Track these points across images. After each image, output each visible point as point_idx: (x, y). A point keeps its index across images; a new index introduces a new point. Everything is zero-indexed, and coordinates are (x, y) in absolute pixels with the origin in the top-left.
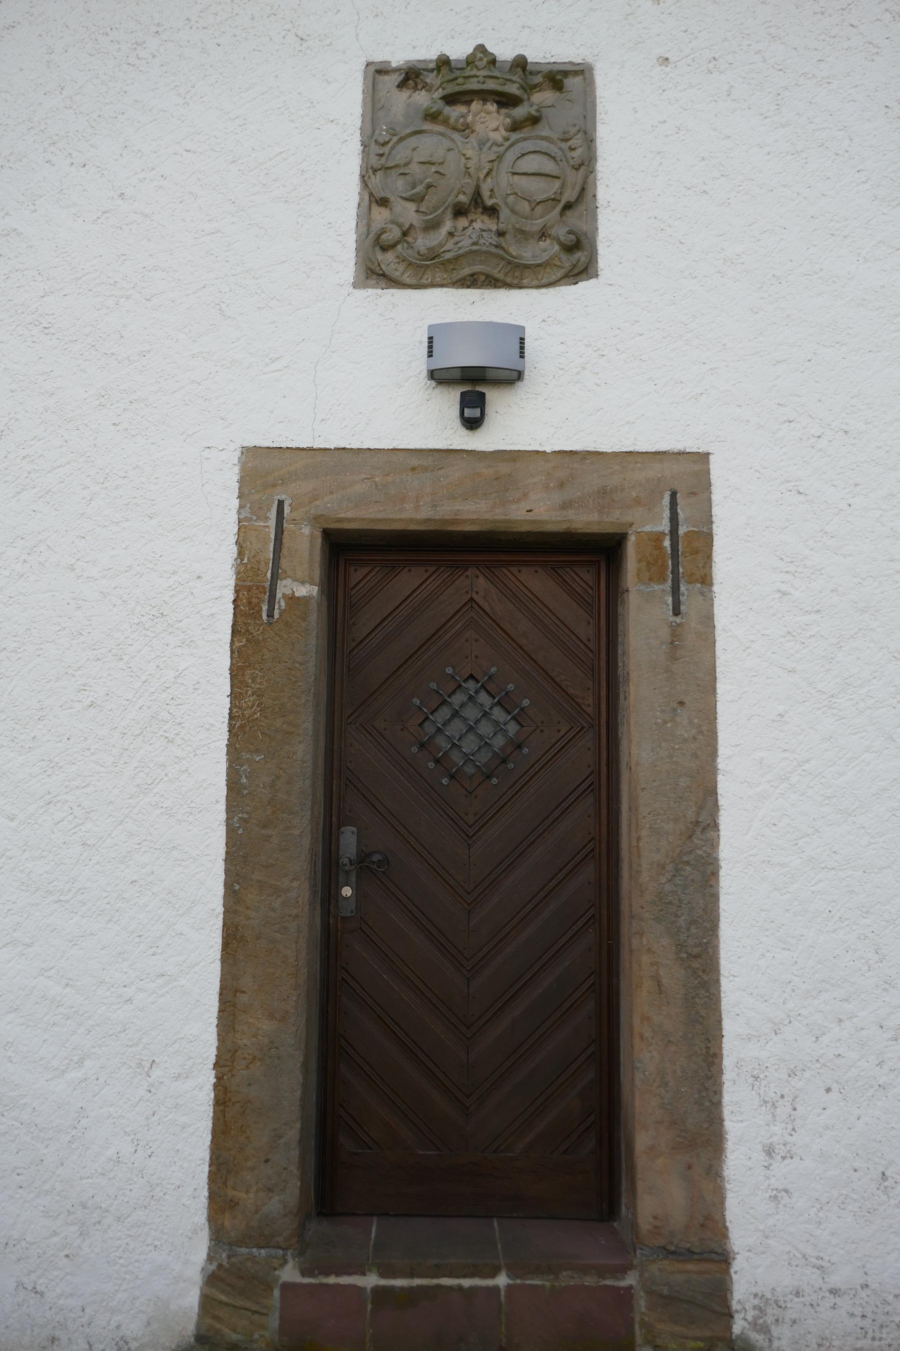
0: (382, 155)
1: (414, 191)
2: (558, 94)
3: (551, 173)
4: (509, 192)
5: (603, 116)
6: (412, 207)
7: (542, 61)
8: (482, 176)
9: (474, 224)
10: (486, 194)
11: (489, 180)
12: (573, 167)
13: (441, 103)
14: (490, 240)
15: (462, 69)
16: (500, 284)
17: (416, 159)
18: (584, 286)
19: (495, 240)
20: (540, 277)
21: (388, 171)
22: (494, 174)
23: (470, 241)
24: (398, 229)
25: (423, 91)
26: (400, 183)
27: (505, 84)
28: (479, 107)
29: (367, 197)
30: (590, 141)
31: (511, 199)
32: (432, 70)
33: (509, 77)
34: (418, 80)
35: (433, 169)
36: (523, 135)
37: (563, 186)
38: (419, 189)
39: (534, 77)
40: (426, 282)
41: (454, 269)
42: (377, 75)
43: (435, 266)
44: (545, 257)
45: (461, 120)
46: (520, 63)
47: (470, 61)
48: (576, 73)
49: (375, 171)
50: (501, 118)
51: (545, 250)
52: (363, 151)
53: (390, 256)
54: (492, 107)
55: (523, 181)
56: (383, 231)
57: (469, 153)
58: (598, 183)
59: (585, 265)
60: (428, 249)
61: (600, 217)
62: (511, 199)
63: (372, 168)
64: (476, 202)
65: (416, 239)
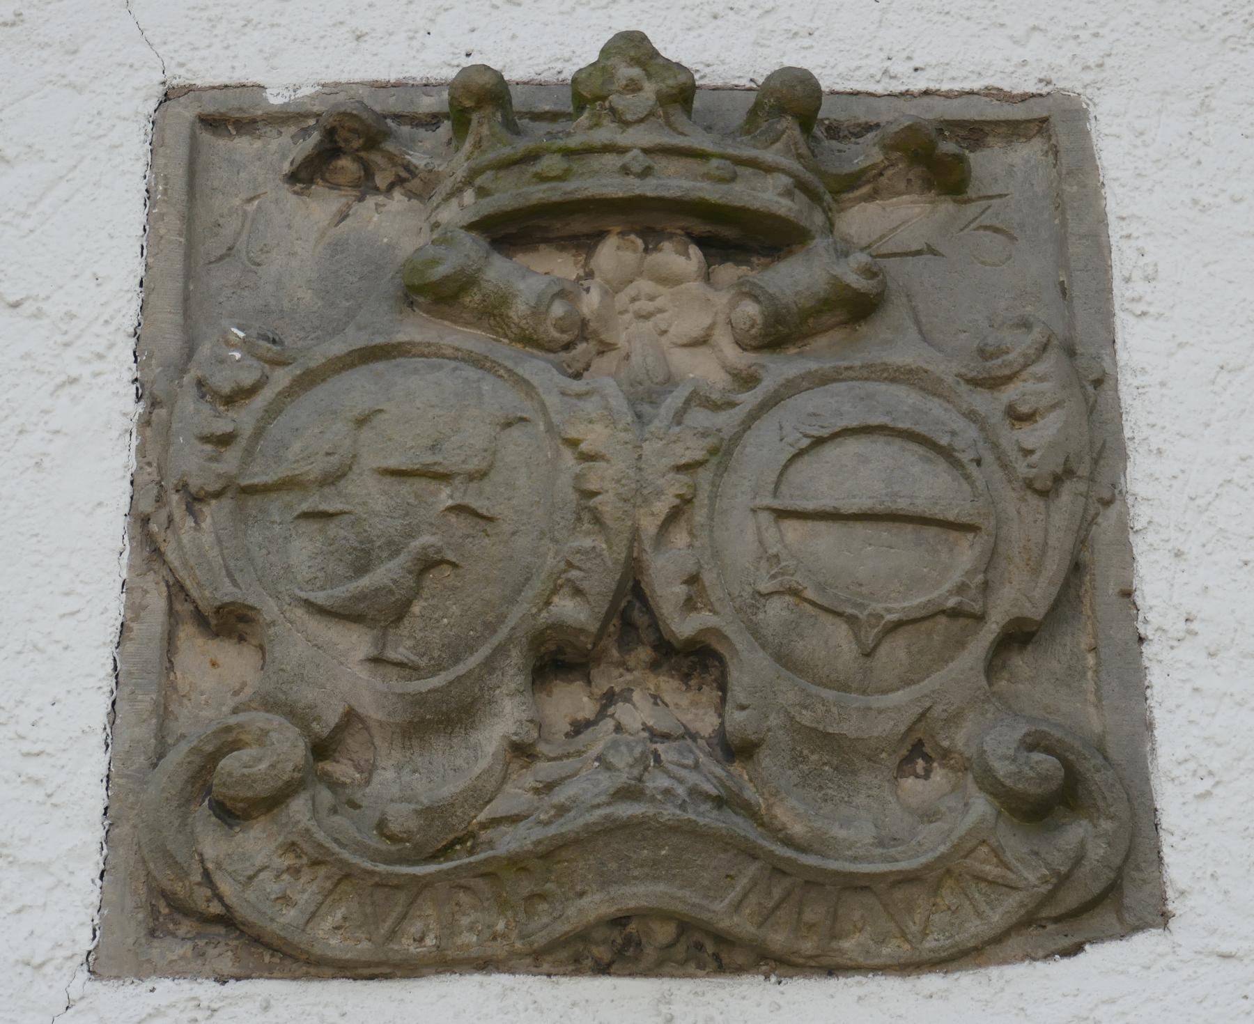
0: (225, 440)
1: (365, 582)
2: (946, 207)
3: (937, 512)
4: (765, 586)
5: (1139, 287)
6: (355, 643)
7: (879, 89)
8: (649, 526)
9: (621, 711)
10: (667, 592)
11: (680, 538)
12: (1029, 485)
13: (471, 248)
14: (693, 778)
15: (553, 116)
16: (740, 959)
17: (370, 460)
18: (1108, 967)
19: (711, 774)
20: (914, 929)
21: (253, 502)
22: (700, 515)
23: (607, 783)
24: (292, 732)
25: (397, 194)
26: (303, 551)
27: (733, 178)
28: (630, 257)
29: (157, 600)
30: (1091, 382)
31: (776, 611)
32: (432, 121)
33: (748, 152)
34: (376, 158)
35: (445, 496)
36: (813, 366)
37: (991, 559)
38: (384, 574)
39: (849, 147)
40: (413, 949)
41: (543, 897)
42: (206, 136)
43: (455, 881)
44: (930, 844)
45: (558, 309)
46: (792, 102)
47: (587, 94)
48: (1015, 130)
49: (194, 500)
50: (722, 299)
51: (929, 815)
52: (145, 422)
53: (257, 843)
54: (683, 261)
55: (824, 543)
56: (228, 741)
57: (594, 437)
58: (1139, 545)
59: (1107, 877)
60: (428, 813)
61: (1155, 677)
62: (776, 611)
63: (182, 488)
64: (628, 624)
65: (369, 771)
